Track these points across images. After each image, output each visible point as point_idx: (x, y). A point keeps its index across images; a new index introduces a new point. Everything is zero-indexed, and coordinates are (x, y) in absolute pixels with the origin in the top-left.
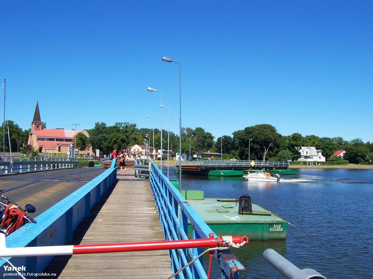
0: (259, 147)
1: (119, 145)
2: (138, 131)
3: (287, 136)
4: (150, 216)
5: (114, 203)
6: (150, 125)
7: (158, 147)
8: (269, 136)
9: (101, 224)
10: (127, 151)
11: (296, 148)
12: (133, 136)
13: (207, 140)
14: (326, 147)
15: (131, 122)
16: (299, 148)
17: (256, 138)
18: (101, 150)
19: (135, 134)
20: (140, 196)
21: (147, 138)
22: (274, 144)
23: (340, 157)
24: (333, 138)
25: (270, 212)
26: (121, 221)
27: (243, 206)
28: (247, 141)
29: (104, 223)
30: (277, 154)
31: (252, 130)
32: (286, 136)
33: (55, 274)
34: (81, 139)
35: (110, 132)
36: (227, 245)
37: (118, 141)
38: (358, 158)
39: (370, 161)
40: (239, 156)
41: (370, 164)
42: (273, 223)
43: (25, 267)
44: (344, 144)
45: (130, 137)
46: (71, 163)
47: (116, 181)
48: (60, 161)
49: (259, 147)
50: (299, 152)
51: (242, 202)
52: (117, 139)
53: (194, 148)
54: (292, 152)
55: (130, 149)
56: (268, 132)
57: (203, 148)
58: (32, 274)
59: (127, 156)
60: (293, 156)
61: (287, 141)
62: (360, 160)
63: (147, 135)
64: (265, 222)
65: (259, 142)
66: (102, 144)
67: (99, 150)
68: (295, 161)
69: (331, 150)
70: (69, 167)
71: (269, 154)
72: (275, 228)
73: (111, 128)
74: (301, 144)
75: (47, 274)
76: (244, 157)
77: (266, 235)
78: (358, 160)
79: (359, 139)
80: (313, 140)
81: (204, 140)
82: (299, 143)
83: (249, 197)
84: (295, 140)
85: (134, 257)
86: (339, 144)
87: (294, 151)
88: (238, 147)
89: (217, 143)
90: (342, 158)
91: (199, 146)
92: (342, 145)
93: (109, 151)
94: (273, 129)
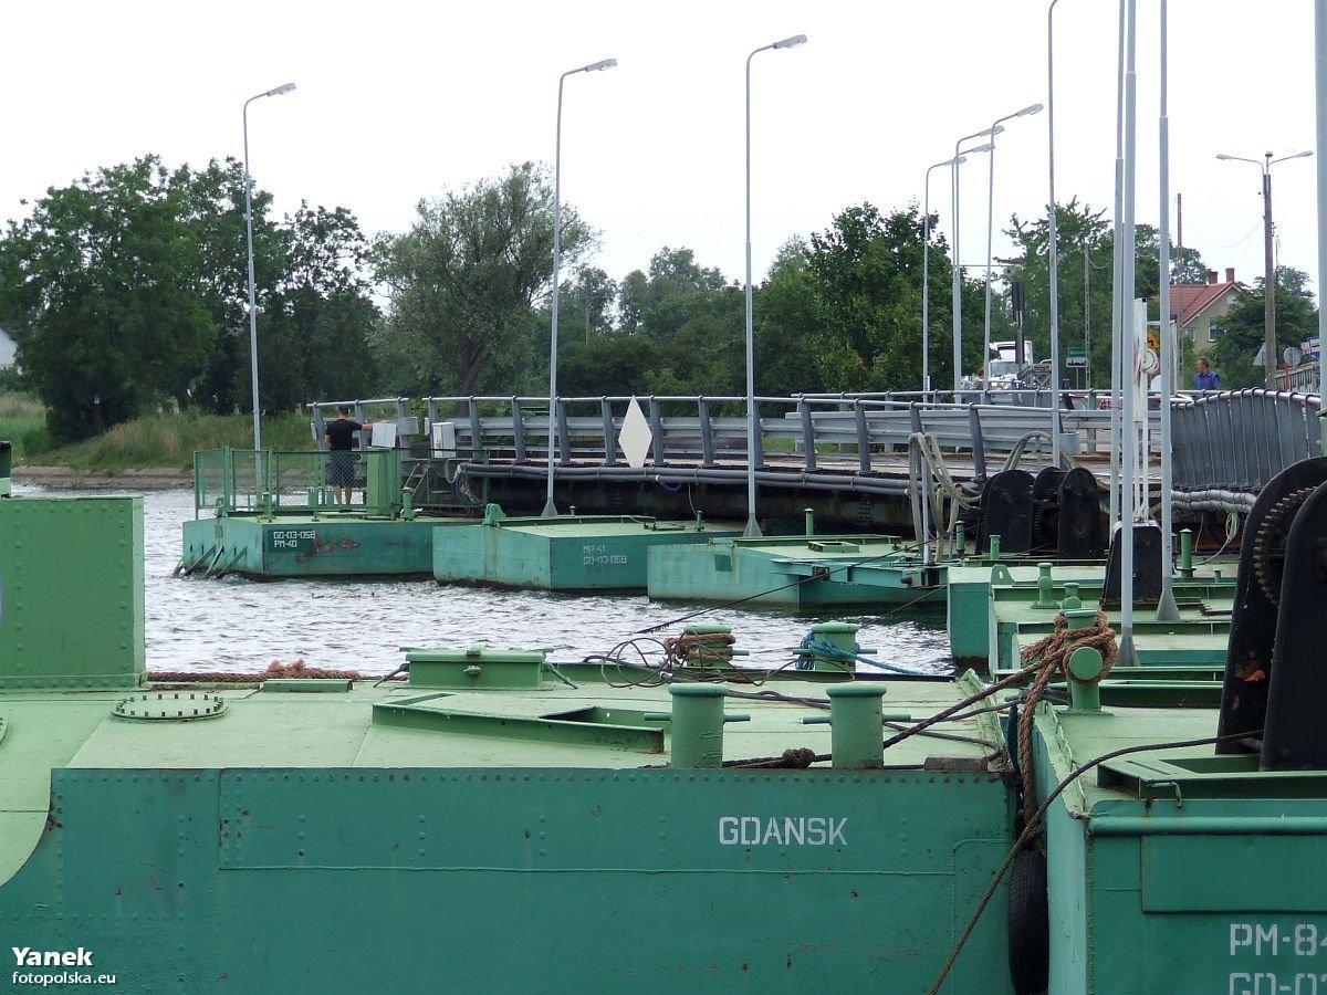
33: (111, 979)
43: (89, 954)
58: (30, 975)
75: (82, 979)
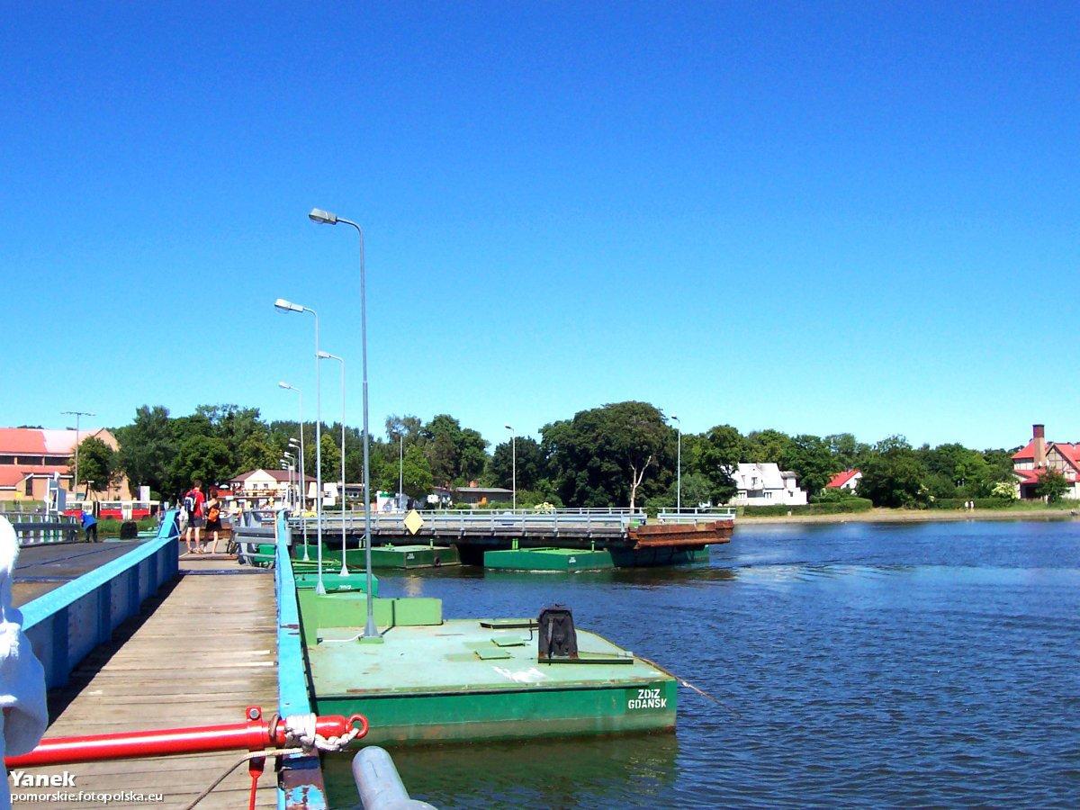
0: (616, 468)
1: (207, 474)
2: (264, 428)
3: (696, 433)
4: (252, 676)
5: (152, 640)
6: (299, 414)
7: (330, 474)
8: (646, 435)
9: (99, 703)
10: (231, 489)
11: (723, 468)
12: (250, 443)
13: (466, 452)
14: (808, 464)
15: (244, 403)
16: (730, 467)
17: (609, 442)
18: (155, 487)
19: (257, 440)
20: (234, 618)
21: (291, 450)
22: (658, 458)
23: (848, 491)
24: (828, 437)
25: (630, 654)
26: (160, 692)
27: (550, 640)
28: (580, 451)
29: (106, 700)
30: (668, 486)
31: (595, 421)
32: (695, 435)
34: (94, 456)
35: (182, 434)
36: (296, 741)
37: (205, 459)
38: (898, 492)
39: (932, 498)
40: (561, 497)
41: (930, 506)
42: (636, 684)
44: (859, 454)
45: (243, 447)
46: (55, 527)
47: (175, 577)
48: (31, 521)
49: (616, 468)
50: (732, 479)
51: (547, 626)
52: (204, 455)
53: (430, 476)
54: (713, 479)
55: (242, 483)
56: (643, 425)
57: (455, 475)
59: (233, 504)
60: (715, 491)
61: (697, 450)
62: (904, 498)
63: (292, 440)
64: (612, 684)
65: (615, 452)
66: (157, 469)
67: (148, 487)
68: (720, 505)
69: (821, 470)
70: (52, 540)
71: (645, 486)
72: (642, 700)
73: (183, 421)
74: (736, 454)
76: (574, 499)
77: (619, 721)
78: (898, 498)
79: (900, 438)
80: (772, 444)
81: (459, 451)
82: (729, 452)
83: (567, 613)
84: (719, 446)
85: (174, 796)
86: (846, 453)
87: (717, 476)
88: (555, 469)
89: (496, 460)
90: (853, 492)
91: (445, 469)
92: (855, 457)
93: (178, 489)
94: (656, 416)
